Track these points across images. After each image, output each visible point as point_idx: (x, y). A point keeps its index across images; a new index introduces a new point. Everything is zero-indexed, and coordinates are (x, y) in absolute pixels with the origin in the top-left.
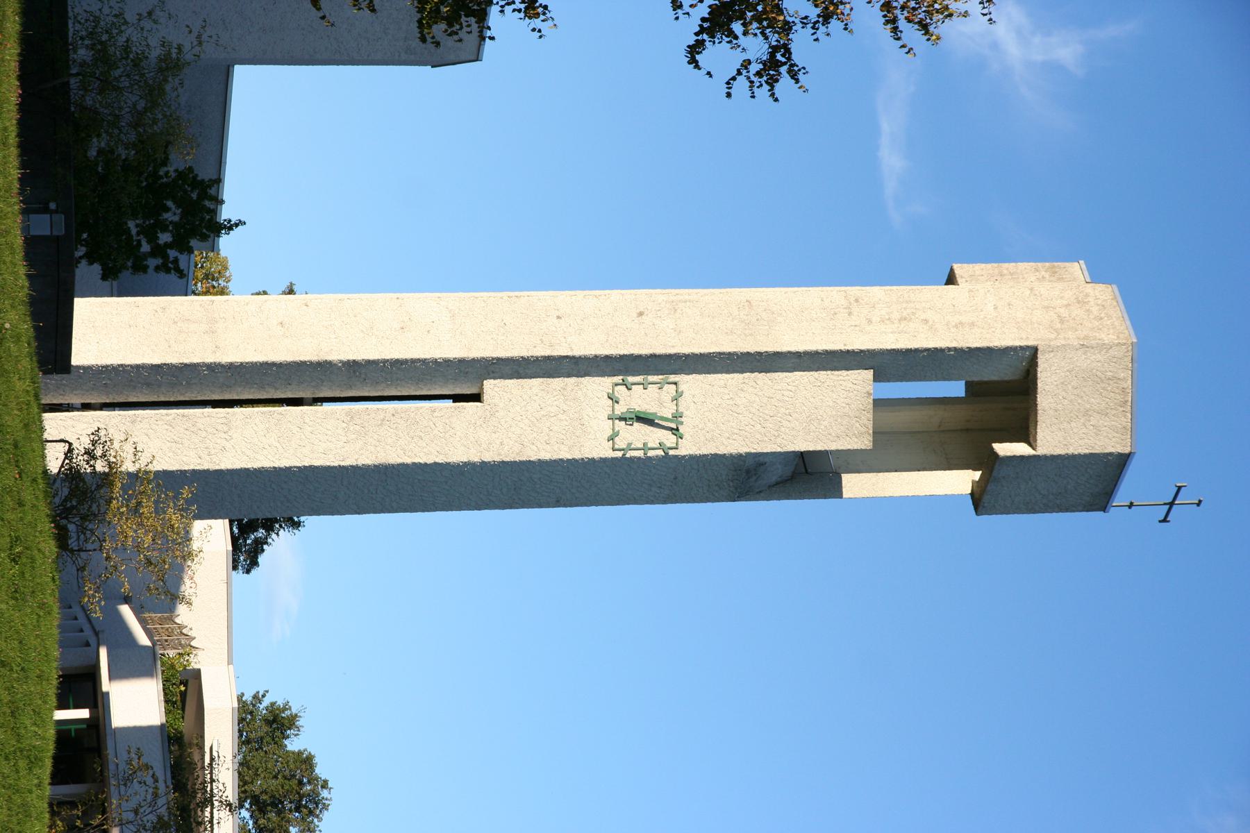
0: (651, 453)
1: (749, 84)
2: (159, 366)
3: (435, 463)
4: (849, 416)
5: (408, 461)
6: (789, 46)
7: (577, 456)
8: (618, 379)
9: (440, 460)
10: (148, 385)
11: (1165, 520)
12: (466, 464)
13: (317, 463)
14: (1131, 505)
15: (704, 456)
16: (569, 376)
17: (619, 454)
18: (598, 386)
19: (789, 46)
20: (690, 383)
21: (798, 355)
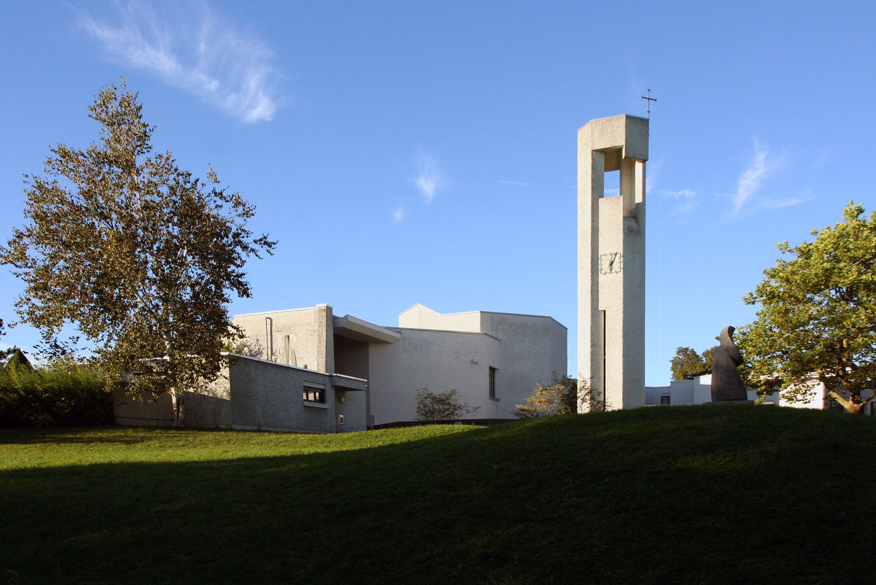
0: (622, 261)
5: (622, 329)
8: (599, 272)
11: (656, 100)
13: (622, 354)
14: (649, 112)
17: (622, 270)
18: (602, 278)
20: (601, 252)
21: (593, 221)
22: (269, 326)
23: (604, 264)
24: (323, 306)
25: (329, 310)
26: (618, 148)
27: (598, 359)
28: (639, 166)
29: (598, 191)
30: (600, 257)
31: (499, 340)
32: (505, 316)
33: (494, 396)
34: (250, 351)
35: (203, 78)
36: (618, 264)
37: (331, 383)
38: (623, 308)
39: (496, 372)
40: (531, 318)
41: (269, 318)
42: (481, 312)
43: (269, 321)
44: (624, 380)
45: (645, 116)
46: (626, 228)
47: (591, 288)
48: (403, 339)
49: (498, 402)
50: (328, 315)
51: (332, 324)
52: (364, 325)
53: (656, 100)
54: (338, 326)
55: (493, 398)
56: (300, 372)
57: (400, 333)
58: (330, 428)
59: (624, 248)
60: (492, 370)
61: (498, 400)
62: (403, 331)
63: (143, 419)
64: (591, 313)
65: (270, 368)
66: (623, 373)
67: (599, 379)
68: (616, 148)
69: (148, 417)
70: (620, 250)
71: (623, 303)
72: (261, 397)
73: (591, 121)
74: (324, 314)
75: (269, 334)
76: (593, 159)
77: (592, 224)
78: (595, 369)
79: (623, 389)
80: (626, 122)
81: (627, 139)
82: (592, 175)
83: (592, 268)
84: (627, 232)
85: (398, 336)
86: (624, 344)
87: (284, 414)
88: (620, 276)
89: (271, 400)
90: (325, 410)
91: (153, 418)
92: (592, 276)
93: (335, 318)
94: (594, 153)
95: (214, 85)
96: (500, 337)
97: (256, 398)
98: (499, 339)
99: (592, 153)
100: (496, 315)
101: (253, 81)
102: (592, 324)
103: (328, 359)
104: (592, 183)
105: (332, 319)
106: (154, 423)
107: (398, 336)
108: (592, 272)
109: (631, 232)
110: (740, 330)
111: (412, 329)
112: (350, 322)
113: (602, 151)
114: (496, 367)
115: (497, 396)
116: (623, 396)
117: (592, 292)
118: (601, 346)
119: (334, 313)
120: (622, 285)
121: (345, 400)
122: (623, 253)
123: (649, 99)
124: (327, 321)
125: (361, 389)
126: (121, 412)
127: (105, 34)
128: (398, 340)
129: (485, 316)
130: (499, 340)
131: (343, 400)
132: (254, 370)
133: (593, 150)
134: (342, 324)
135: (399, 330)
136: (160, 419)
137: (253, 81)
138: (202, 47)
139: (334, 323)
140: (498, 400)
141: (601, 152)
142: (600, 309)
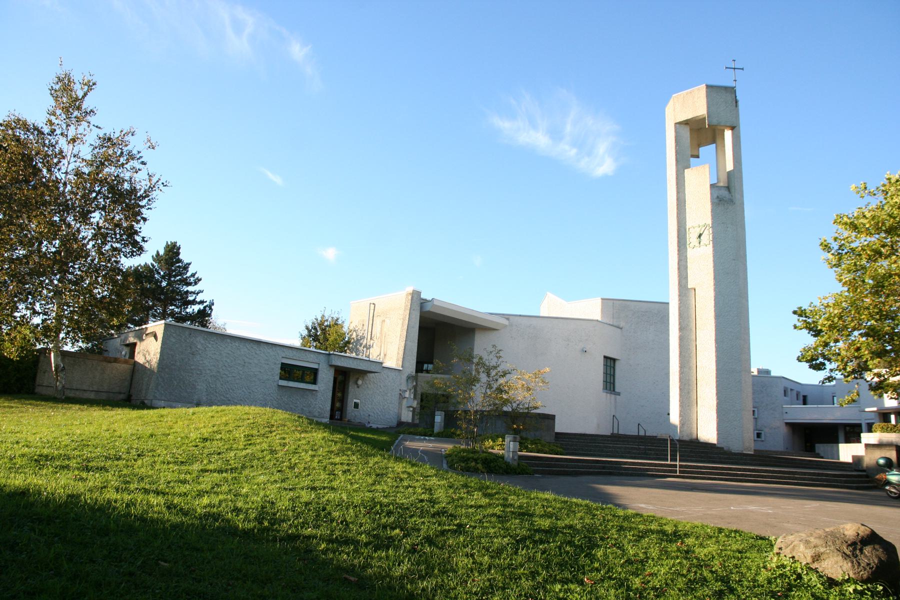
0: (711, 232)
1: (213, 307)
2: (680, 389)
3: (714, 300)
4: (452, 589)
5: (713, 309)
6: (169, 243)
7: (712, 255)
8: (688, 246)
9: (713, 299)
10: (689, 393)
11: (743, 69)
12: (715, 290)
13: (714, 338)
14: (735, 81)
15: (712, 215)
16: (687, 261)
17: (711, 242)
18: (690, 253)
19: (169, 243)
20: (689, 223)
21: (678, 192)
22: (372, 311)
23: (692, 237)
24: (410, 289)
25: (416, 295)
26: (701, 117)
27: (689, 345)
28: (728, 134)
29: (682, 164)
30: (687, 230)
31: (621, 329)
32: (626, 302)
33: (614, 390)
34: (357, 336)
35: (567, 147)
36: (707, 237)
37: (329, 362)
38: (714, 285)
39: (617, 363)
40: (657, 305)
41: (373, 304)
42: (602, 299)
43: (372, 306)
44: (717, 370)
45: (732, 84)
46: (715, 196)
47: (678, 263)
48: (511, 325)
49: (618, 396)
50: (415, 298)
51: (419, 308)
52: (450, 308)
53: (743, 69)
54: (424, 310)
55: (613, 392)
56: (278, 348)
57: (508, 319)
58: (319, 412)
59: (712, 219)
60: (610, 362)
61: (619, 394)
62: (511, 318)
63: (77, 390)
64: (679, 292)
65: (229, 340)
66: (716, 361)
67: (690, 368)
68: (697, 119)
69: (85, 388)
70: (709, 221)
71: (714, 278)
72: (208, 372)
73: (673, 95)
74: (410, 297)
75: (371, 318)
76: (676, 132)
77: (677, 196)
78: (684, 356)
79: (717, 381)
80: (707, 91)
81: (708, 108)
82: (676, 147)
83: (679, 242)
84: (716, 201)
85: (505, 322)
86: (716, 326)
87: (243, 393)
88: (710, 249)
89: (224, 376)
90: (314, 392)
91: (91, 389)
92: (678, 250)
93: (423, 302)
94: (678, 125)
95: (574, 151)
96: (622, 324)
97: (199, 373)
98: (621, 326)
99: (675, 126)
100: (618, 302)
101: (602, 148)
102: (680, 304)
103: (408, 342)
104: (676, 155)
105: (419, 302)
106: (92, 396)
107: (505, 322)
108: (679, 246)
109: (720, 201)
110: (823, 301)
111: (520, 316)
112: (436, 305)
113: (686, 123)
114: (616, 358)
115: (617, 390)
116: (717, 390)
117: (679, 269)
118: (691, 329)
119: (423, 296)
120: (712, 259)
121: (362, 383)
122: (712, 224)
123: (734, 69)
124: (411, 305)
125: (374, 371)
126: (44, 381)
127: (505, 125)
128: (506, 326)
129: (607, 302)
130: (621, 329)
131: (360, 382)
132: (203, 342)
133: (676, 123)
134: (428, 308)
135: (507, 317)
136: (103, 392)
137: (602, 148)
138: (568, 128)
139: (421, 308)
140: (619, 394)
141: (686, 124)
142: (689, 287)
